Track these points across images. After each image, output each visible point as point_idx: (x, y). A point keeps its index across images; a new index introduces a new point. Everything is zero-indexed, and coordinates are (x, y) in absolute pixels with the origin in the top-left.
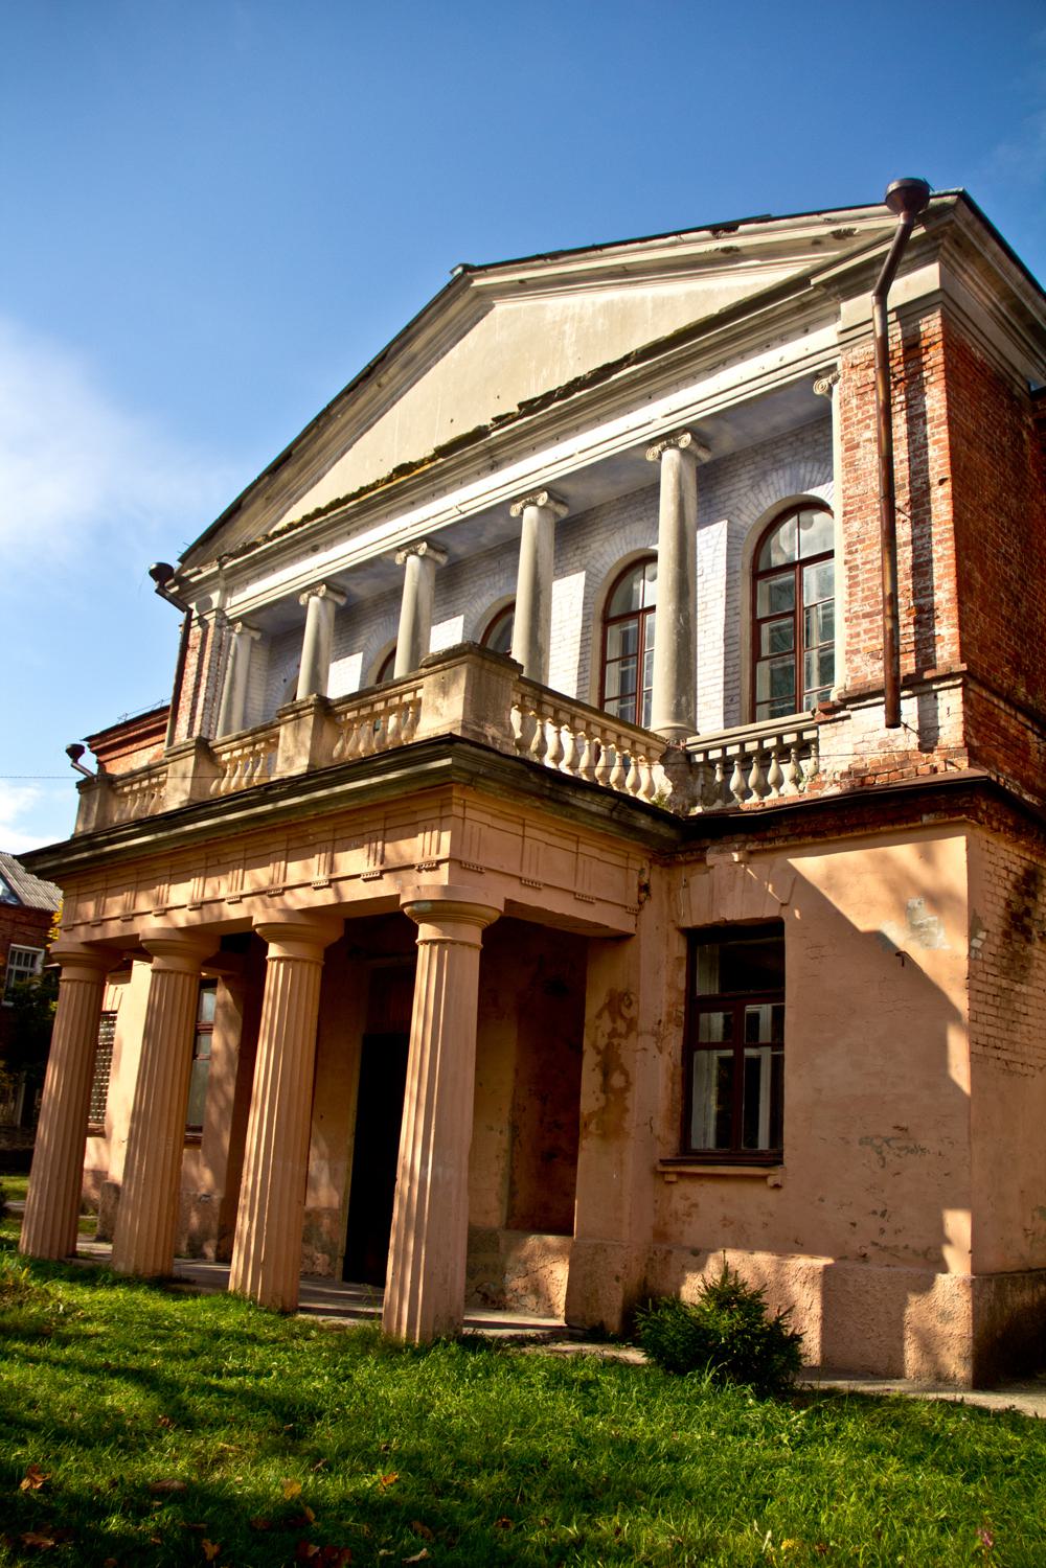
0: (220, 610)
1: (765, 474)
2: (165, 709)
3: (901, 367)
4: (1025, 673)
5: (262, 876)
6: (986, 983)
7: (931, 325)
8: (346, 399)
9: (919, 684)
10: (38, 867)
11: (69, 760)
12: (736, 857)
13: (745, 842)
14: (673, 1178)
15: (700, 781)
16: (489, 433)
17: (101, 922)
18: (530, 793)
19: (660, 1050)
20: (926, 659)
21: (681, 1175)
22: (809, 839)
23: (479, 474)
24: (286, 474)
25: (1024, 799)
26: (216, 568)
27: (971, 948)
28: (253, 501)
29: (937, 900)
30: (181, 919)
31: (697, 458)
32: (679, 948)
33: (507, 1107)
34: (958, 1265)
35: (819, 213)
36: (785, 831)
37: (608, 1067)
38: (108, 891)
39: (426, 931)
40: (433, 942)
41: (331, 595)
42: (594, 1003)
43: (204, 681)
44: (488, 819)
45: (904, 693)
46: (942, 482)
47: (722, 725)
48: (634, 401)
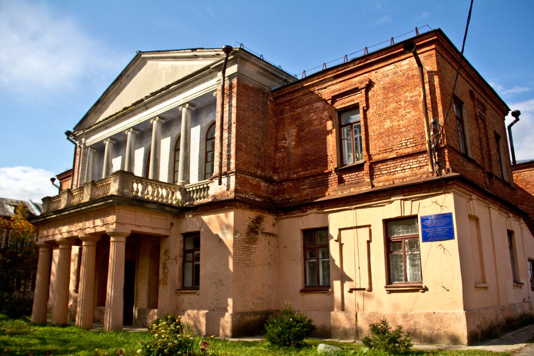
0: (85, 144)
1: (208, 113)
2: (71, 170)
3: (228, 92)
4: (261, 167)
5: (80, 225)
6: (240, 246)
7: (235, 81)
8: (112, 86)
9: (227, 174)
10: (32, 222)
11: (51, 182)
12: (191, 216)
13: (192, 213)
14: (179, 294)
15: (188, 196)
16: (144, 101)
17: (48, 236)
18: (134, 205)
19: (177, 263)
20: (229, 169)
21: (181, 293)
22: (205, 212)
23: (144, 111)
24: (99, 106)
25: (256, 201)
26: (82, 132)
27: (234, 238)
28: (91, 114)
29: (228, 227)
30: (65, 235)
31: (191, 109)
32: (181, 238)
33: (147, 278)
34: (230, 310)
35: (213, 49)
36: (199, 210)
37: (165, 267)
38: (49, 228)
39: (112, 239)
40: (115, 241)
41: (111, 141)
42: (162, 252)
43: (81, 164)
44: (126, 212)
45: (223, 177)
46: (234, 123)
47: (197, 180)
48: (176, 94)
